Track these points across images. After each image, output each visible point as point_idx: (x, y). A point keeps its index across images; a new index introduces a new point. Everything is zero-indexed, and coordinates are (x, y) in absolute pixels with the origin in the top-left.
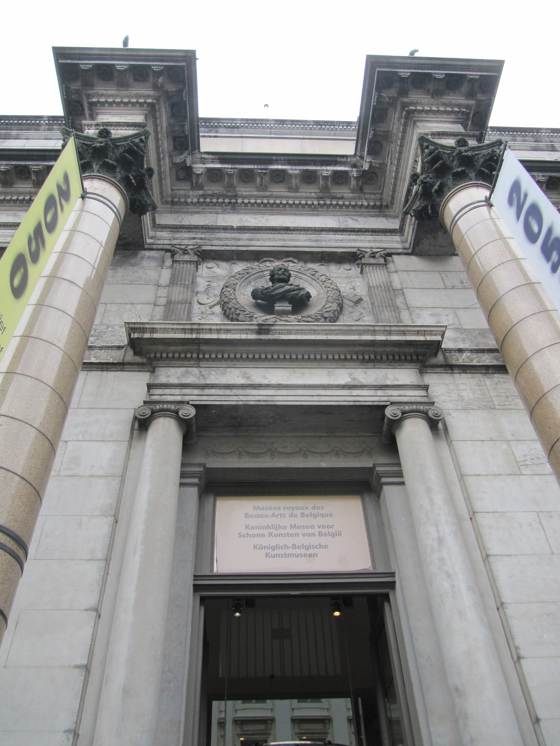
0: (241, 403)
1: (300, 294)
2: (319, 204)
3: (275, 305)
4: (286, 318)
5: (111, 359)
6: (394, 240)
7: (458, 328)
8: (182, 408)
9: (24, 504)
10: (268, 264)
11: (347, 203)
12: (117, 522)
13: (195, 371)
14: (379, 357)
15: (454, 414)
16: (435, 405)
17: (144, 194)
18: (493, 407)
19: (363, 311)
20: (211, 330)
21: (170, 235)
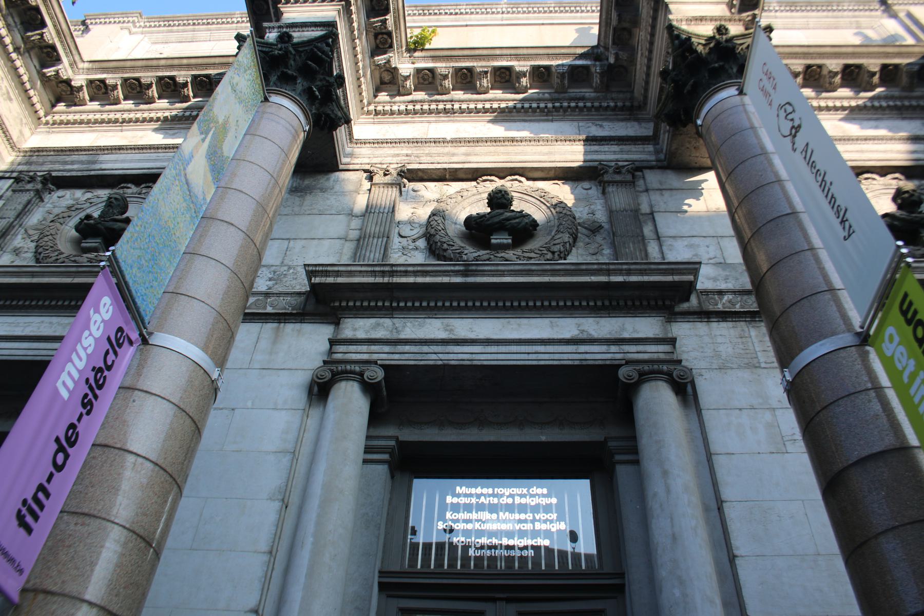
0: (440, 363)
1: (523, 223)
2: (554, 107)
3: (491, 237)
4: (503, 255)
5: (290, 308)
6: (646, 150)
7: (720, 263)
8: (368, 369)
9: (156, 494)
10: (487, 184)
11: (589, 104)
12: (286, 507)
13: (387, 322)
14: (614, 303)
15: (707, 375)
16: (683, 364)
17: (335, 106)
18: (757, 365)
19: (602, 242)
20: (406, 272)
21: (369, 152)
